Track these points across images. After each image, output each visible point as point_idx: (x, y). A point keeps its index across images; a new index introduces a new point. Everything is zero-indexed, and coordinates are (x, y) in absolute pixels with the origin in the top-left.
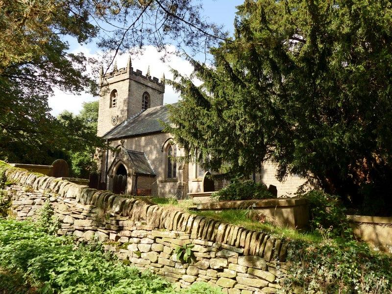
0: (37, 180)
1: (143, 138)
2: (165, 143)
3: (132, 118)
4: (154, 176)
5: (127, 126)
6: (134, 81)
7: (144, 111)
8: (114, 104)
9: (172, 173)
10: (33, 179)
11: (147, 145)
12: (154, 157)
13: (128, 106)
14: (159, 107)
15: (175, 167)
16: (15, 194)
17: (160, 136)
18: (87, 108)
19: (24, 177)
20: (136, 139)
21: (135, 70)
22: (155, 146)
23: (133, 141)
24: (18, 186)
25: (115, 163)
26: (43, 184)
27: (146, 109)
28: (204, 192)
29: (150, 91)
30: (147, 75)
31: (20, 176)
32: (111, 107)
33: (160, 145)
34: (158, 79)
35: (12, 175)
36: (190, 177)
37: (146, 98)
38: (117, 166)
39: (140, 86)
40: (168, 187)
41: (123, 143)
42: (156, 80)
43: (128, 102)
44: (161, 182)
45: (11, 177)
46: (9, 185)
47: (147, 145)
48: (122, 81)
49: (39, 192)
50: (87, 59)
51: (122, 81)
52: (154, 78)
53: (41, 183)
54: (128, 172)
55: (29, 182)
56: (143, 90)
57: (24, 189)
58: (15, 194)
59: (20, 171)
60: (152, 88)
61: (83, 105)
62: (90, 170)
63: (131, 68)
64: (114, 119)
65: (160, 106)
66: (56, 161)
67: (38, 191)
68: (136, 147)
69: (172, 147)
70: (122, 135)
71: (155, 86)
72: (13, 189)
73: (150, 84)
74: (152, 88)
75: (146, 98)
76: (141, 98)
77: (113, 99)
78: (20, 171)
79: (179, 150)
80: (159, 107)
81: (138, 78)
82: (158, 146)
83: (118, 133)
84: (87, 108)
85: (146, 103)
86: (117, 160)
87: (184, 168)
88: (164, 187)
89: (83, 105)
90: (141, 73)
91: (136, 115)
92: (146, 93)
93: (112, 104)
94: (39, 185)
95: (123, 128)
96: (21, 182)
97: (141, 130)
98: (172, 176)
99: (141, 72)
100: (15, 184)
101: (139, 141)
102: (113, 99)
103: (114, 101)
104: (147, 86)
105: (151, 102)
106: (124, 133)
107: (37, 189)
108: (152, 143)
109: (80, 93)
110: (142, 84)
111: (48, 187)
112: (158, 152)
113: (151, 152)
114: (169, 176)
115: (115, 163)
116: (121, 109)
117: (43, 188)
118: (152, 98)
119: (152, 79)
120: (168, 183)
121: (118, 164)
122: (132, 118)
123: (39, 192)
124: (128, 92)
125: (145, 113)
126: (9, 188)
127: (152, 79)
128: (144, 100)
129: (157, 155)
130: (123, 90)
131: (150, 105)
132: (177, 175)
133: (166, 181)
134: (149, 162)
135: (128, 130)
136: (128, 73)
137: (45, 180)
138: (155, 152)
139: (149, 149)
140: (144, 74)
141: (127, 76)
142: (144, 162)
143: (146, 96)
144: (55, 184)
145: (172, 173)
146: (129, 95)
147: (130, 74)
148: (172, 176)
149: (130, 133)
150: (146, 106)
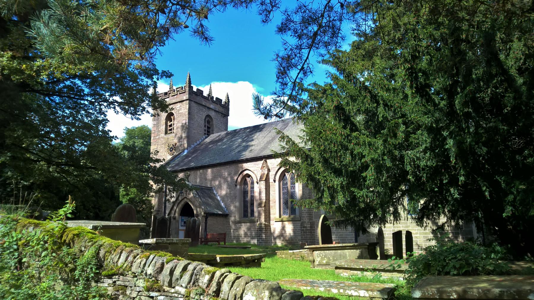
0: (167, 268)
1: (209, 170)
2: (239, 175)
3: (193, 146)
4: (226, 216)
5: (187, 156)
6: (195, 102)
7: (206, 138)
8: (171, 130)
9: (249, 210)
10: (158, 265)
11: (214, 178)
12: (224, 192)
13: (188, 133)
14: (223, 133)
15: (252, 204)
16: (122, 293)
17: (232, 168)
18: (130, 134)
19: (139, 260)
20: (201, 171)
21: (195, 89)
22: (225, 179)
23: (197, 174)
24: (129, 277)
25: (178, 202)
26: (181, 277)
27: (209, 135)
28: (322, 244)
29: (212, 114)
30: (209, 95)
31: (130, 259)
32: (166, 133)
33: (232, 178)
34: (221, 100)
35: (114, 256)
36: (272, 216)
37: (208, 122)
38: (180, 206)
39: (201, 107)
40: (243, 229)
41: (187, 177)
42: (219, 100)
43: (188, 128)
44: (235, 223)
45: (113, 259)
46: (110, 277)
47: (214, 178)
48: (180, 102)
49: (176, 293)
50: (160, 72)
51: (180, 102)
52: (217, 98)
53: (177, 272)
54: (195, 212)
55: (150, 270)
56: (203, 114)
57: (141, 283)
58: (122, 293)
59: (128, 249)
60: (215, 111)
61: (125, 131)
62: (143, 210)
63: (191, 88)
64: (171, 148)
65: (225, 132)
66: (245, 256)
67: (173, 290)
68: (200, 181)
69: (248, 179)
70: (182, 166)
71: (218, 108)
72: (118, 283)
73: (212, 106)
74: (215, 111)
75: (208, 122)
76: (202, 122)
77: (169, 124)
78: (128, 249)
79: (258, 183)
80: (223, 133)
81: (198, 99)
82: (229, 179)
83: (177, 165)
84: (130, 134)
85: (208, 128)
86: (180, 198)
87: (265, 206)
88: (237, 229)
89: (125, 131)
90: (202, 93)
91: (198, 142)
92: (208, 116)
93: (168, 130)
94: (174, 279)
95: (183, 161)
96: (134, 269)
97: (206, 161)
98: (249, 215)
99: (202, 91)
100: (123, 275)
101: (205, 174)
102: (169, 124)
103: (171, 126)
104: (209, 108)
105: (214, 126)
106: (185, 165)
107: (170, 285)
108: (221, 176)
109: (140, 117)
110: (203, 105)
111: (194, 283)
112: (229, 187)
113: (220, 187)
114: (245, 215)
115: (178, 202)
116: (179, 135)
117: (184, 285)
118: (215, 122)
119: (215, 99)
120: (243, 224)
121: (183, 203)
122: (193, 146)
123: (176, 293)
124: (187, 116)
125: (208, 140)
126: (110, 281)
127: (215, 99)
128: (206, 124)
129: (228, 190)
130: (181, 112)
131: (213, 130)
132: (256, 214)
133: (240, 222)
134: (219, 198)
135: (190, 161)
136: (187, 93)
137: (185, 269)
138: (225, 187)
139: (217, 183)
140: (205, 94)
141: (186, 96)
142: (214, 198)
143: (208, 120)
144: (207, 277)
145: (249, 210)
146: (190, 119)
147: (189, 94)
148: (249, 215)
149: (193, 164)
150: (208, 133)
